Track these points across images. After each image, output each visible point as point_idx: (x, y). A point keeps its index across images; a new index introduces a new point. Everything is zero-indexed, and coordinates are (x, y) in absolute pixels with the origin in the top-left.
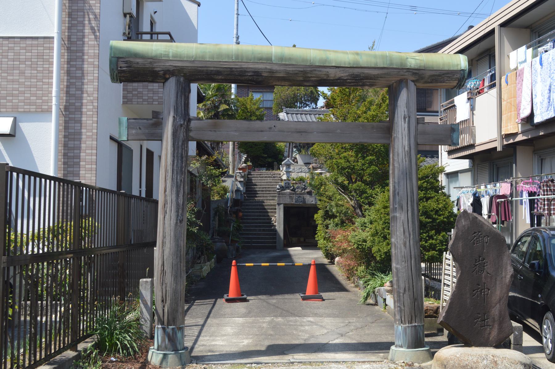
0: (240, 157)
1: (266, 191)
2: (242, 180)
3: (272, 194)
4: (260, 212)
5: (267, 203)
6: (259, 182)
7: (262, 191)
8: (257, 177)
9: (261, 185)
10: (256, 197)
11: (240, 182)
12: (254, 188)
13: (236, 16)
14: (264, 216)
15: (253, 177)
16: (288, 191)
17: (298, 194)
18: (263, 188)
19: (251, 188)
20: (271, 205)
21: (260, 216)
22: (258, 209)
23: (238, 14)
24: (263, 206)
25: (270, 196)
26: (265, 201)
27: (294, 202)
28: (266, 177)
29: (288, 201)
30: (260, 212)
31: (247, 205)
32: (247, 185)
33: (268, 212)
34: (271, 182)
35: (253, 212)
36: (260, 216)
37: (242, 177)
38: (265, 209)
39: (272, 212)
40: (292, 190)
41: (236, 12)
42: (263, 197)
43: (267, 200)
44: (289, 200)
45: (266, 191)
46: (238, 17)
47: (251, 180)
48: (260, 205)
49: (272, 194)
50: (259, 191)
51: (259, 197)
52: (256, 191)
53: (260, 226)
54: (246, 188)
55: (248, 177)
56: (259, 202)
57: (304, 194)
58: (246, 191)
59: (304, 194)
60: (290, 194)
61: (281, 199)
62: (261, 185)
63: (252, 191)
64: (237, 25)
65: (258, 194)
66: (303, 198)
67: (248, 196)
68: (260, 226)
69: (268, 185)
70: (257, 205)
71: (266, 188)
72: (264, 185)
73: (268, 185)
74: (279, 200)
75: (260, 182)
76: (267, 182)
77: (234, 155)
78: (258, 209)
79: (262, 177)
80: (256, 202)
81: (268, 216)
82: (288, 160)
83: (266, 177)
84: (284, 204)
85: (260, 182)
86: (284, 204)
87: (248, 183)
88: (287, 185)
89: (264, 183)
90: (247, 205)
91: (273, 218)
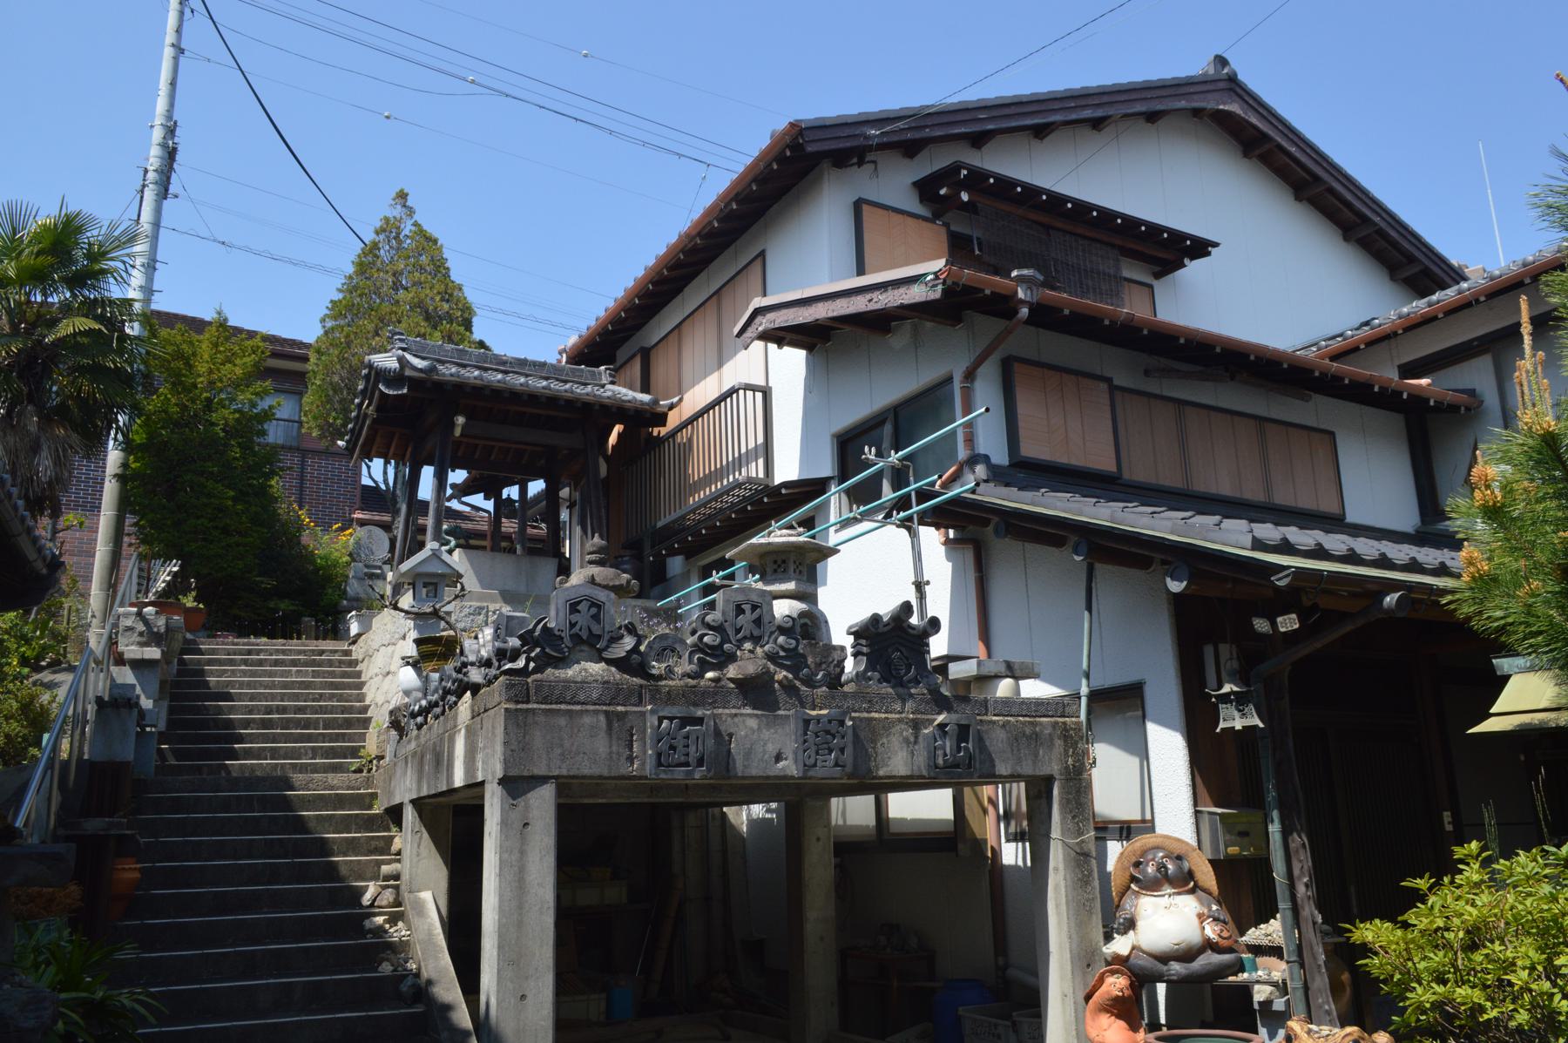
0: (146, 579)
1: (286, 724)
2: (154, 653)
3: (324, 738)
4: (270, 849)
5: (306, 786)
6: (242, 685)
7: (266, 724)
8: (232, 662)
9: (253, 698)
10: (234, 755)
11: (138, 665)
12: (220, 710)
13: (168, 52)
14: (302, 874)
15: (210, 662)
16: (596, 668)
17: (670, 698)
18: (269, 710)
19: (199, 710)
20: (340, 802)
21: (274, 874)
22: (254, 826)
23: (179, 50)
24: (287, 803)
25: (315, 753)
26: (298, 778)
27: (643, 762)
28: (276, 663)
29: (591, 752)
30: (270, 849)
31: (177, 805)
32: (173, 697)
33: (324, 847)
34: (308, 685)
35: (219, 850)
36: (274, 874)
37: (152, 638)
38: (300, 825)
39: (352, 846)
40: (621, 664)
41: (170, 38)
42: (274, 754)
43: (303, 769)
44: (601, 745)
45: (286, 724)
46: (176, 59)
47: (202, 673)
48: (266, 803)
49: (324, 738)
50: (247, 724)
51: (248, 754)
52: (230, 724)
53: (281, 964)
54: (171, 710)
55: (182, 662)
56: (252, 781)
57: (715, 695)
58: (171, 723)
59: (715, 695)
60: (614, 693)
61: (538, 739)
62: (253, 698)
63: (204, 724)
64: (173, 84)
65: (241, 739)
66: (717, 733)
67: (179, 754)
68: (281, 964)
69: (296, 697)
70: (249, 803)
71: (284, 710)
72: (273, 697)
73: (296, 697)
74: (516, 749)
75: (249, 685)
76: (285, 685)
77: (111, 586)
78: (254, 826)
79: (260, 663)
80: (235, 783)
81: (332, 871)
82: (435, 555)
83: (276, 663)
84: (564, 786)
85: (249, 685)
86: (564, 786)
87: (184, 686)
88: (582, 619)
89: (273, 685)
90: (177, 805)
91: (371, 890)
